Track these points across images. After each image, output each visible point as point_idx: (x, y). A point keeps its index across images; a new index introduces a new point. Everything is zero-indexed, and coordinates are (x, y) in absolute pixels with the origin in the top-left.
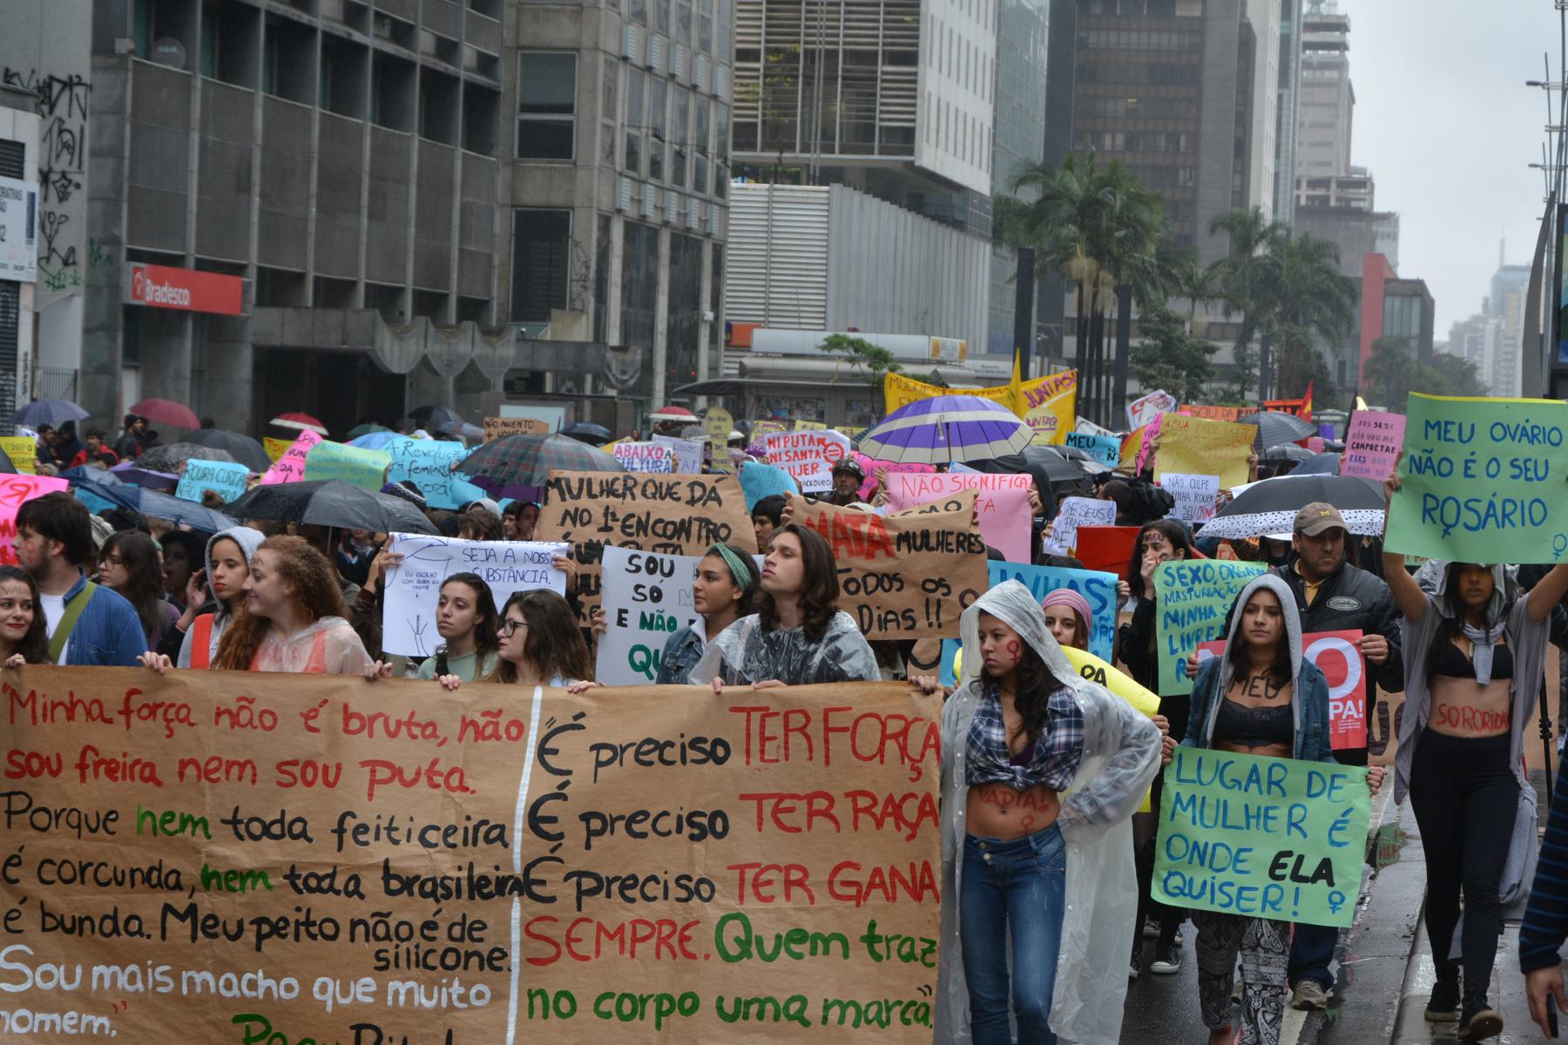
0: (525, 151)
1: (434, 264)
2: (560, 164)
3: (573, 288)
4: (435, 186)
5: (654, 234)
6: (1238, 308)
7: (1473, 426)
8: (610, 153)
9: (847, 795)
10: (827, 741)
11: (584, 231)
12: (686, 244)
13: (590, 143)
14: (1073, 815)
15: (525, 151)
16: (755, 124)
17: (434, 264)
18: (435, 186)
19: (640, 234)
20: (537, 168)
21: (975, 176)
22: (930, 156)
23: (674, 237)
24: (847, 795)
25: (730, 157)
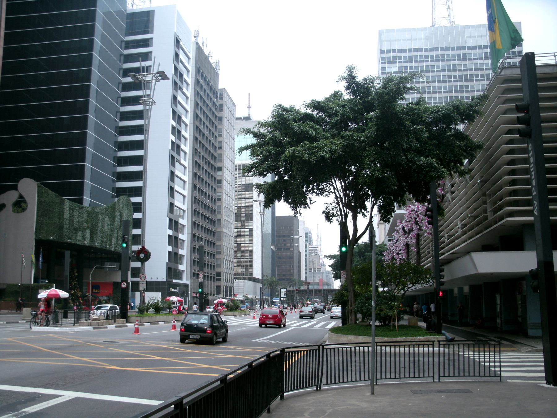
0: (217, 281)
1: (211, 291)
2: (219, 282)
3: (221, 292)
4: (211, 285)
5: (228, 287)
6: (380, 280)
7: (155, 57)
8: (224, 281)
9: (437, 341)
10: (412, 345)
11: (222, 287)
12: (231, 288)
13: (222, 280)
14: (401, 257)
15: (217, 281)
16: (132, 277)
17: (211, 291)
18: (211, 285)
19: (227, 287)
20: (218, 282)
21: (260, 277)
22: (255, 276)
23: (226, 286)
24: (437, 341)
25: (129, 281)
